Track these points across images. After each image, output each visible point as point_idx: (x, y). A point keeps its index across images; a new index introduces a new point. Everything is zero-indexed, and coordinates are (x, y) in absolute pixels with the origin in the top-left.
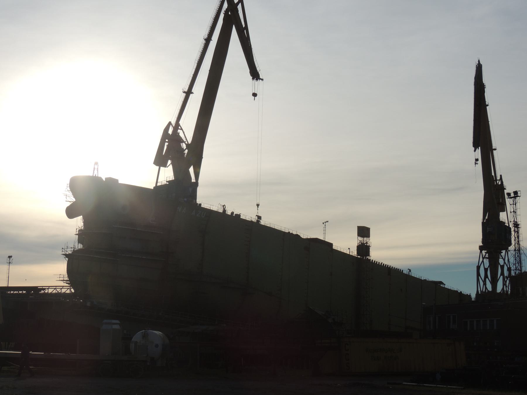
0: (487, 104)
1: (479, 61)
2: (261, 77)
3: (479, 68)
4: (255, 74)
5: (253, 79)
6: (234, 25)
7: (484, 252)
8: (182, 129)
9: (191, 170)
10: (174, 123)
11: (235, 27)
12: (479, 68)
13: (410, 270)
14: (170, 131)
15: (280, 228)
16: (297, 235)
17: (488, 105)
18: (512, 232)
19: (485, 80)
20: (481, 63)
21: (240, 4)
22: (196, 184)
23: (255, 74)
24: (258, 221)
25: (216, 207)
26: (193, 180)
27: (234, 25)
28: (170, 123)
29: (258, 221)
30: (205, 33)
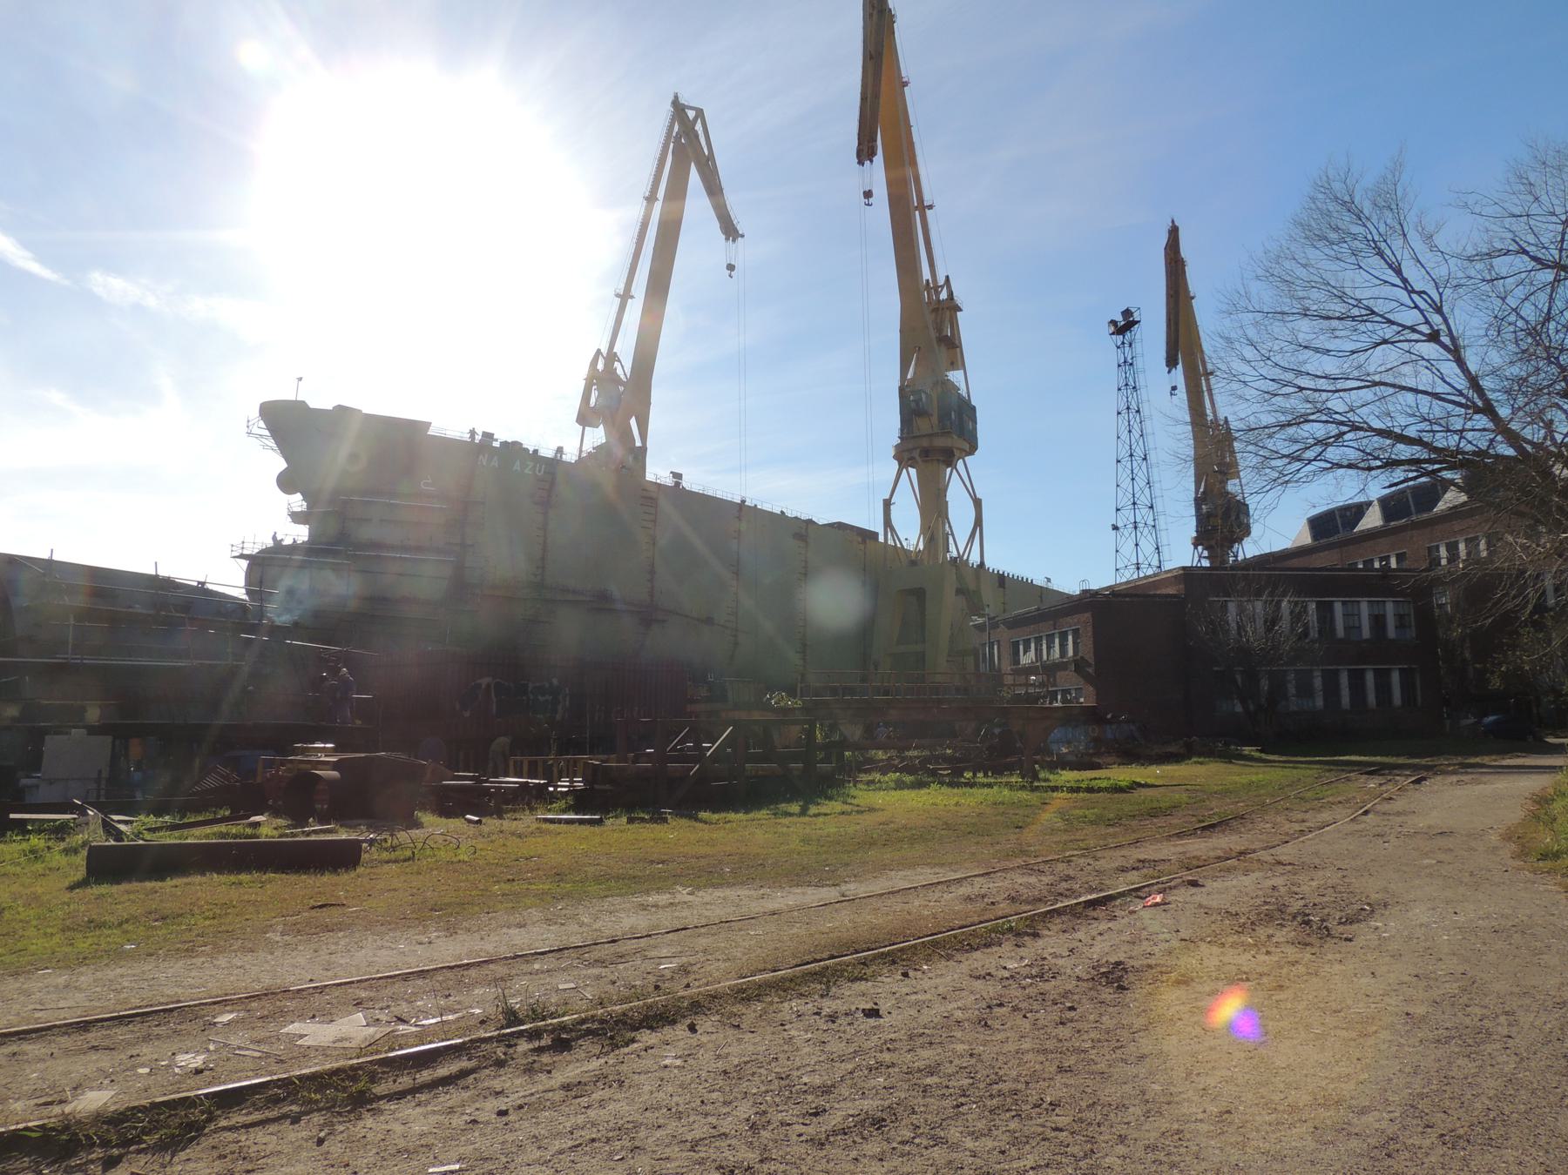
0: (1192, 295)
1: (1173, 222)
2: (740, 232)
3: (1174, 232)
4: (730, 230)
5: (727, 239)
6: (693, 164)
7: (1200, 548)
8: (619, 361)
9: (633, 422)
10: (604, 351)
11: (698, 171)
12: (1174, 232)
13: (1049, 580)
14: (600, 366)
15: (729, 495)
16: (796, 518)
17: (1193, 298)
18: (1420, 483)
19: (1185, 251)
20: (1176, 224)
21: (699, 121)
22: (644, 449)
23: (730, 230)
24: (677, 484)
25: (695, 489)
26: (638, 443)
27: (693, 164)
28: (599, 352)
29: (677, 484)
30: (645, 189)
